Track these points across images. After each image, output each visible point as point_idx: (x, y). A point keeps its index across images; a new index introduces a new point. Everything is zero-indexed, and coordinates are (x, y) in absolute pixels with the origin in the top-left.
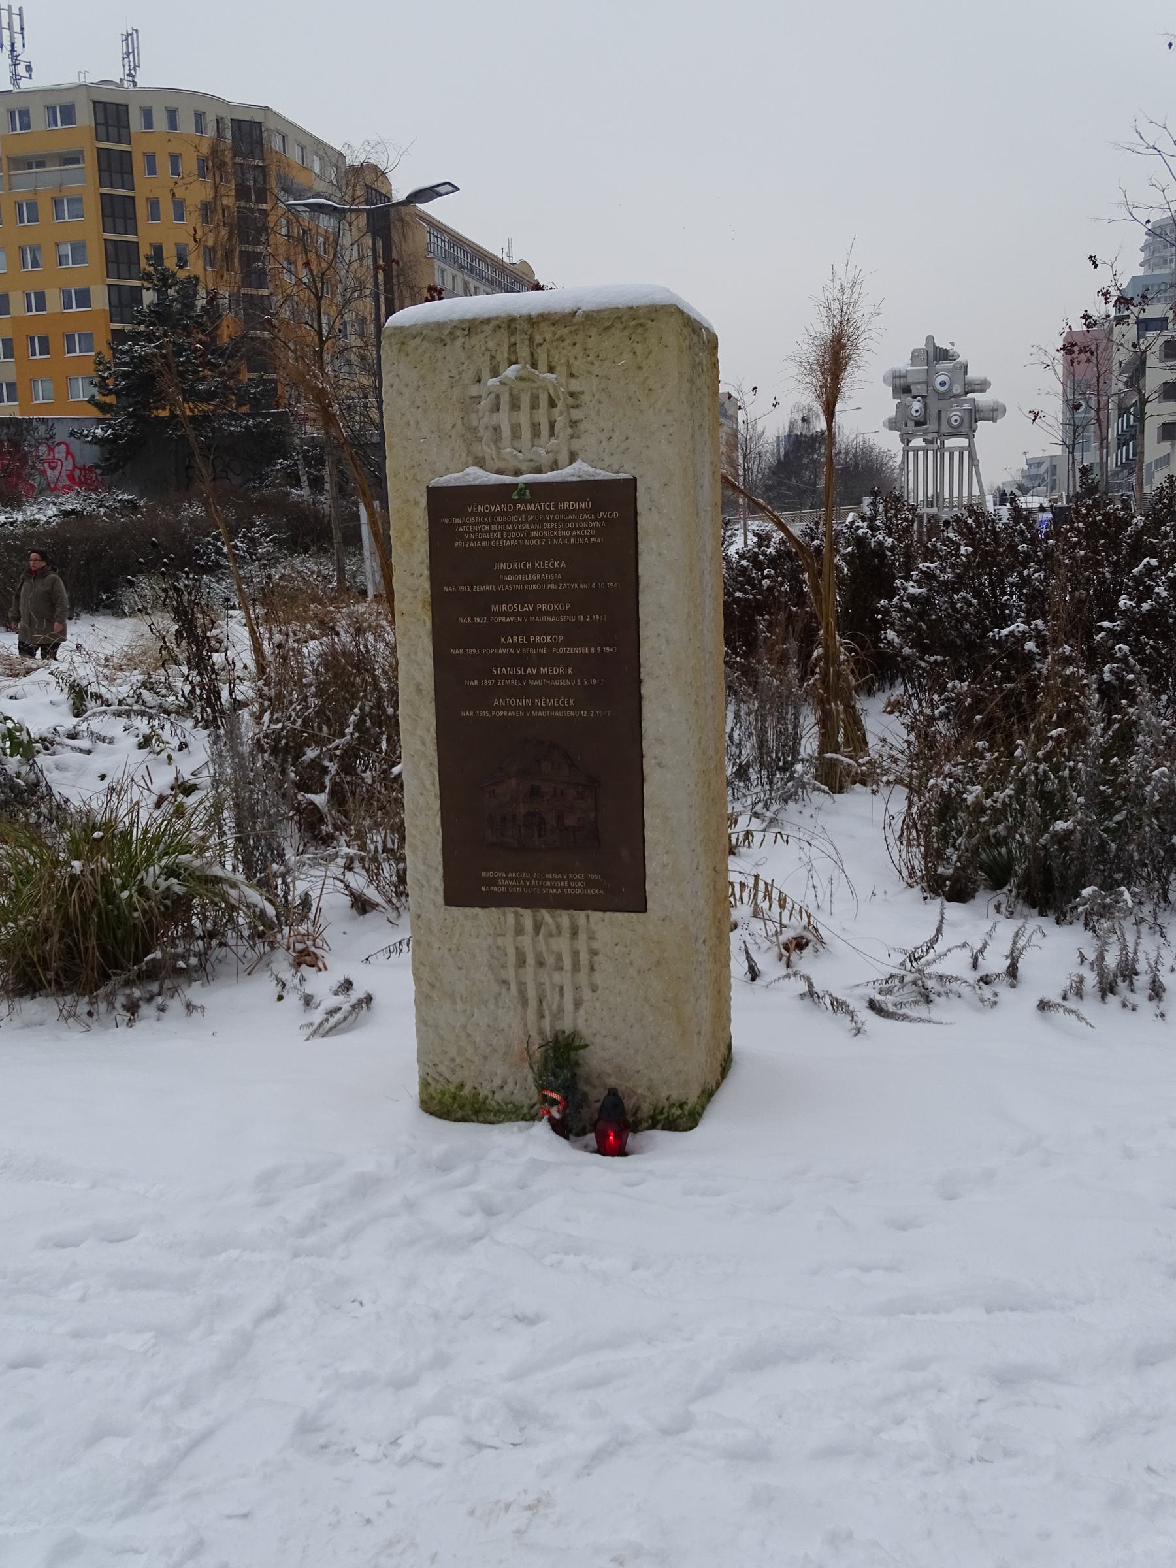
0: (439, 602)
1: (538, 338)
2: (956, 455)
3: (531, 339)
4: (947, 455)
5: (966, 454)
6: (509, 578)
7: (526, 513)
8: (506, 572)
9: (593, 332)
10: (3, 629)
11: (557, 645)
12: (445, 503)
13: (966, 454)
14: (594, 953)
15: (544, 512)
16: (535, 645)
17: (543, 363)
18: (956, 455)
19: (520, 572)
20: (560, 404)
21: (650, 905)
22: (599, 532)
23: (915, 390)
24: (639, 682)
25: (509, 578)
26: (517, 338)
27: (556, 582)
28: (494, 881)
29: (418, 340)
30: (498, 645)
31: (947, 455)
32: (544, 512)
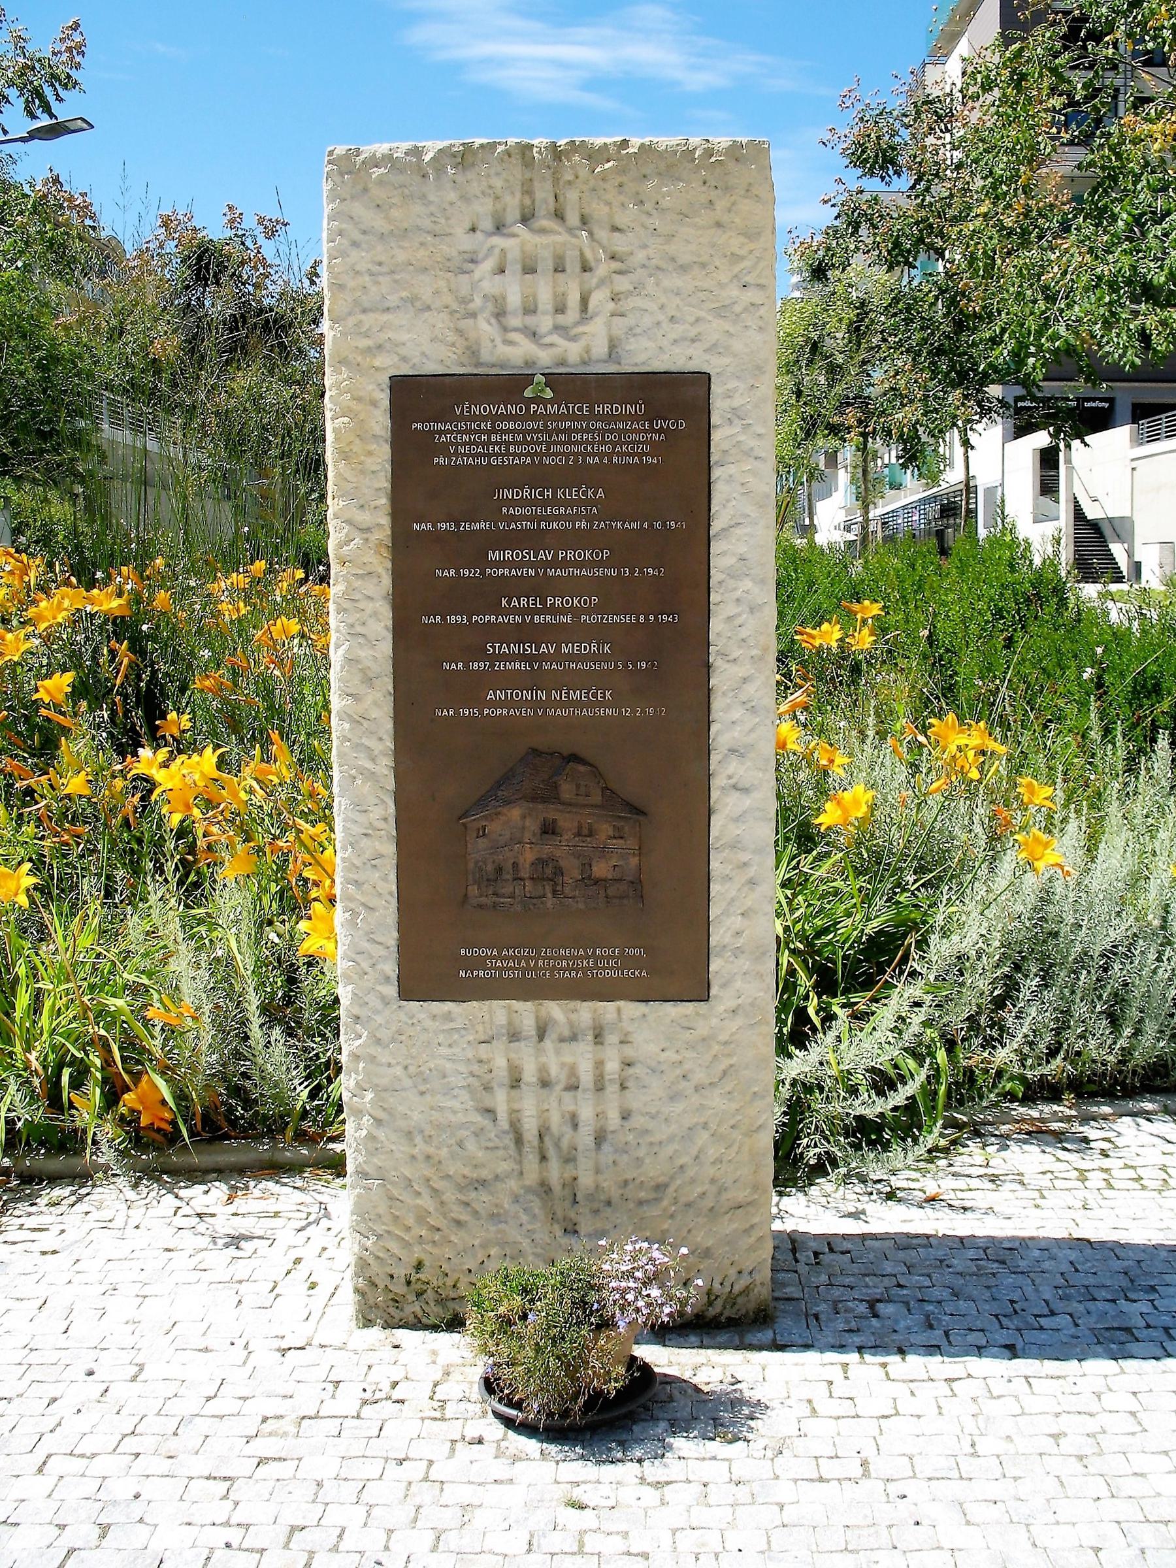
0: (404, 545)
8: (511, 503)
11: (588, 612)
12: (418, 401)
15: (574, 418)
16: (554, 611)
19: (533, 503)
27: (590, 519)
28: (480, 963)
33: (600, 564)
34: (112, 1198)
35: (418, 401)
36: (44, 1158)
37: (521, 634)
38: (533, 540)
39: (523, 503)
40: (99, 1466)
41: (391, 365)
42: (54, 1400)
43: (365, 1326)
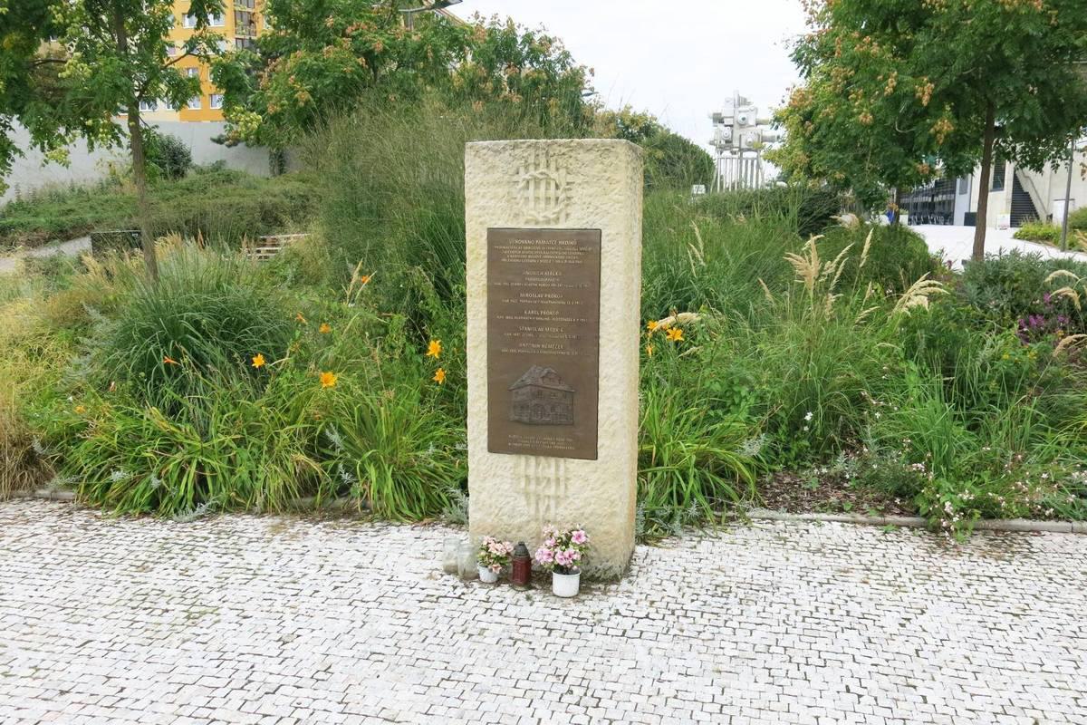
0: (492, 290)
1: (551, 153)
2: (750, 162)
3: (547, 153)
4: (744, 162)
5: (755, 162)
6: (531, 279)
7: (541, 246)
8: (529, 276)
9: (581, 151)
10: (3, 248)
11: (555, 316)
12: (496, 237)
13: (755, 162)
14: (568, 479)
15: (551, 245)
16: (543, 316)
17: (553, 166)
18: (750, 162)
19: (536, 276)
20: (561, 188)
21: (495, 455)
22: (580, 258)
23: (727, 121)
24: (598, 337)
25: (531, 279)
26: (540, 152)
27: (556, 283)
28: (516, 441)
29: (485, 151)
30: (523, 314)
31: (744, 162)
32: (551, 245)
33: (559, 300)
34: (636, 448)
35: (496, 237)
36: (2, 500)
37: (531, 323)
38: (538, 290)
39: (533, 276)
40: (369, 605)
41: (487, 226)
42: (138, 700)
43: (798, 58)
